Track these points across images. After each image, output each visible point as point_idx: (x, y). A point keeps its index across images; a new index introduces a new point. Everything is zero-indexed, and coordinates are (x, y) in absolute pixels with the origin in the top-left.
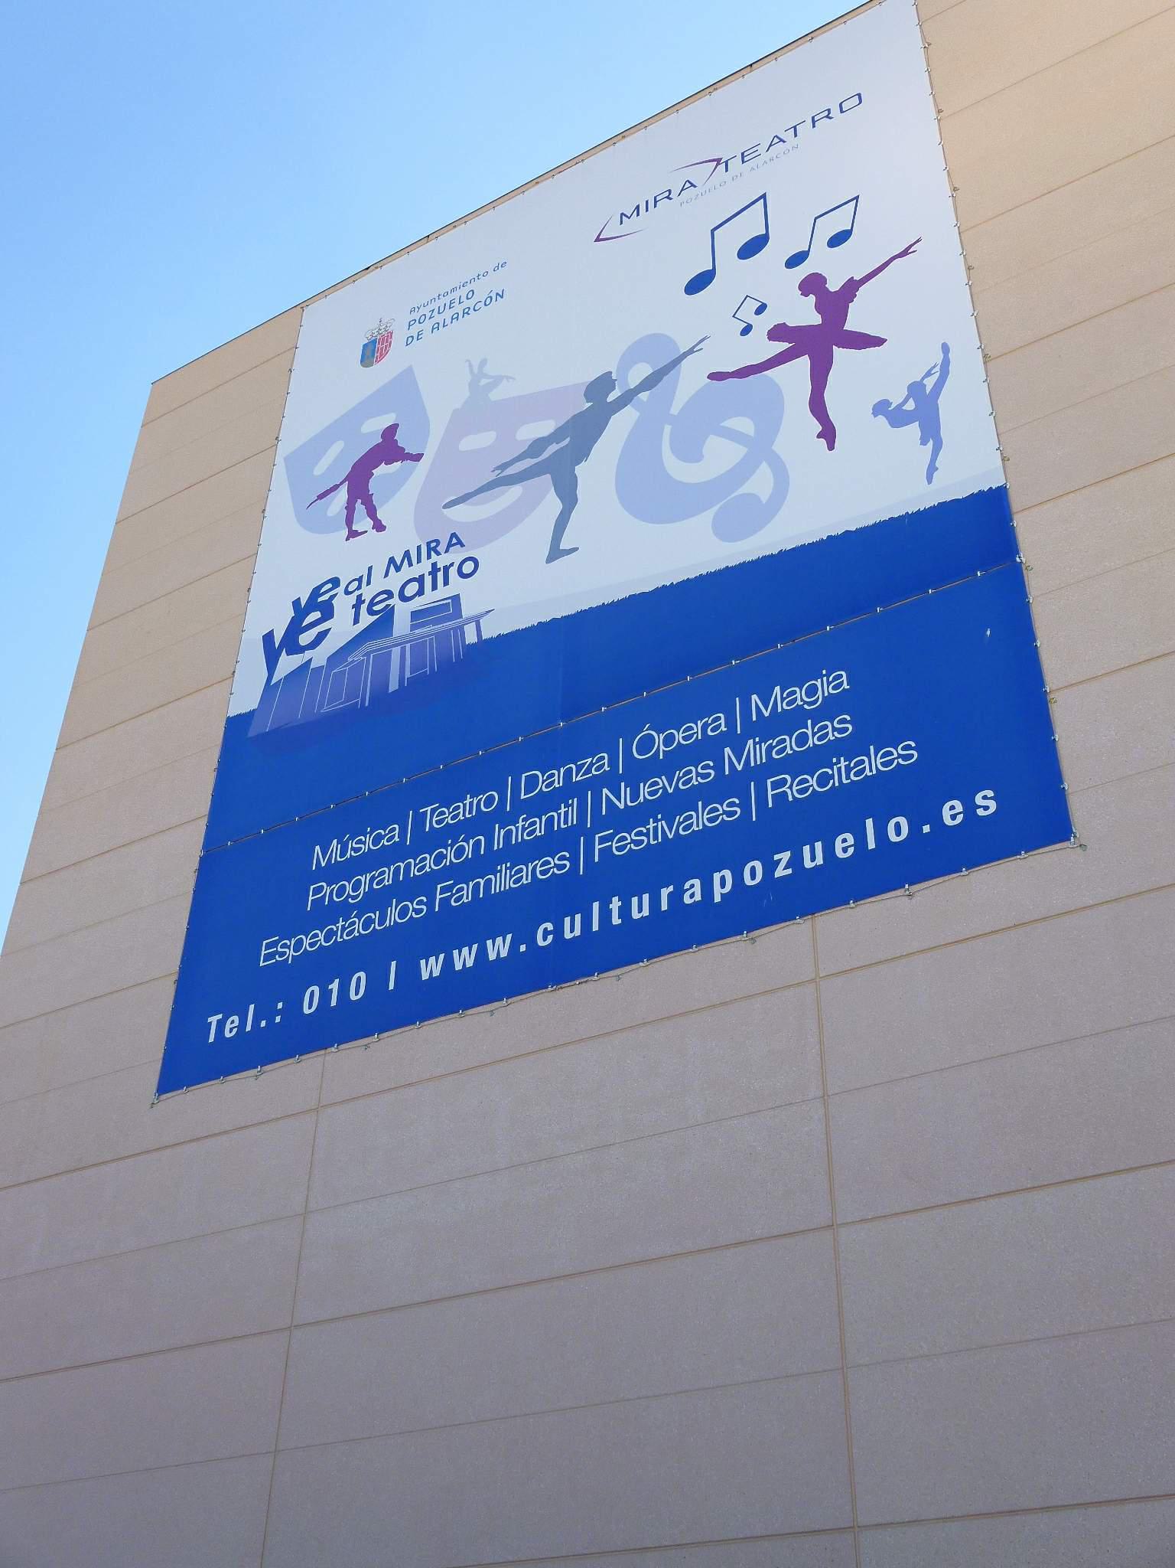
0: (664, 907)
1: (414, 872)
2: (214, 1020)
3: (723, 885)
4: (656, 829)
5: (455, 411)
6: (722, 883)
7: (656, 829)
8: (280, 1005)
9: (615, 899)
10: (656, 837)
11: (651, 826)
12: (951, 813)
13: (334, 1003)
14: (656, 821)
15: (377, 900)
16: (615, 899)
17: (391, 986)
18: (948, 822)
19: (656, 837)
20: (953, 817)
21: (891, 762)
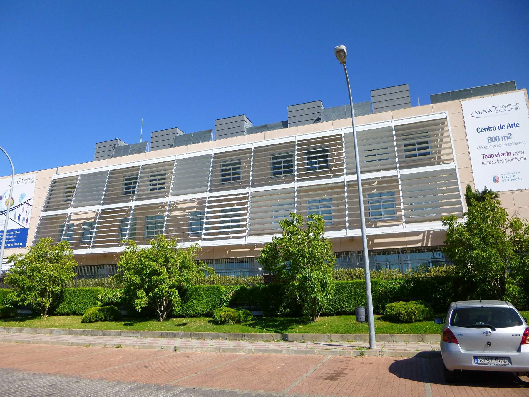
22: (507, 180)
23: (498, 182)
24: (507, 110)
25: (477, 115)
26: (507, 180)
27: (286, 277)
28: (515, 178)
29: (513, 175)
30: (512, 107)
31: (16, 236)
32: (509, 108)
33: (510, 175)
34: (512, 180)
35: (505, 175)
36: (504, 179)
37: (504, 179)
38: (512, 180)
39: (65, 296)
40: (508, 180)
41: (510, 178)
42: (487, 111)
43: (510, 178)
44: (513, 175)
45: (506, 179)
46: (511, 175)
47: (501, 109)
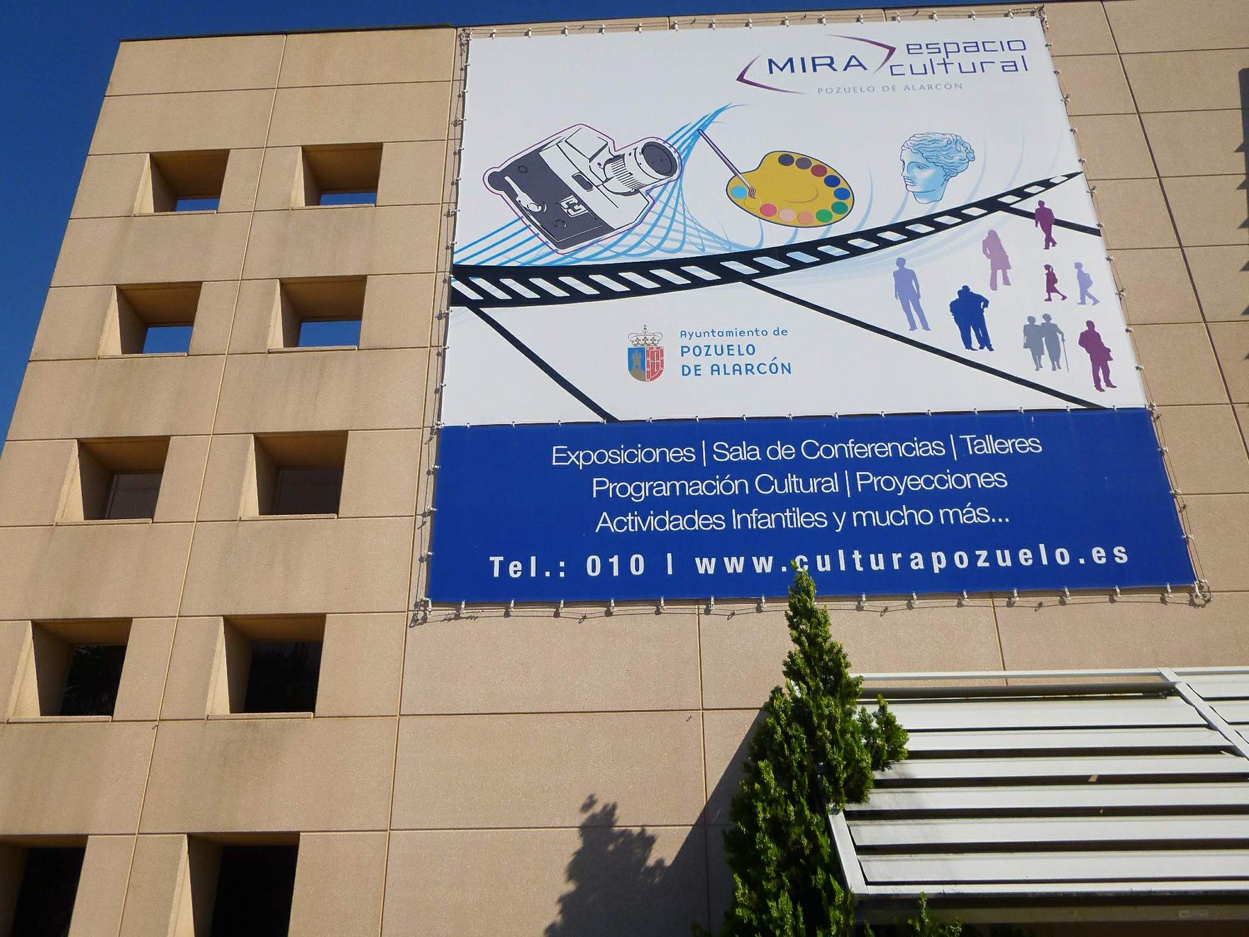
0: (896, 567)
1: (689, 492)
2: (497, 560)
3: (940, 562)
4: (633, 521)
5: (1082, 334)
6: (939, 562)
7: (633, 521)
8: (562, 564)
9: (856, 552)
10: (633, 527)
11: (630, 518)
12: (1098, 555)
13: (616, 573)
14: (791, 511)
15: (654, 505)
16: (856, 552)
17: (670, 572)
18: (512, 575)
19: (633, 527)
20: (515, 572)
21: (810, 523)
22: (705, 370)
23: (655, 373)
24: (953, 69)
25: (781, 78)
26: (705, 370)
27: (750, 920)
28: (754, 360)
29: (744, 342)
30: (982, 56)
31: (994, 480)
32: (967, 59)
33: (726, 341)
34: (736, 369)
35: (702, 342)
36: (690, 359)
37: (690, 359)
38: (736, 369)
39: (790, 904)
40: (715, 369)
41: (729, 361)
42: (840, 63)
43: (729, 361)
44: (744, 342)
45: (705, 363)
46: (726, 341)
47: (919, 61)
